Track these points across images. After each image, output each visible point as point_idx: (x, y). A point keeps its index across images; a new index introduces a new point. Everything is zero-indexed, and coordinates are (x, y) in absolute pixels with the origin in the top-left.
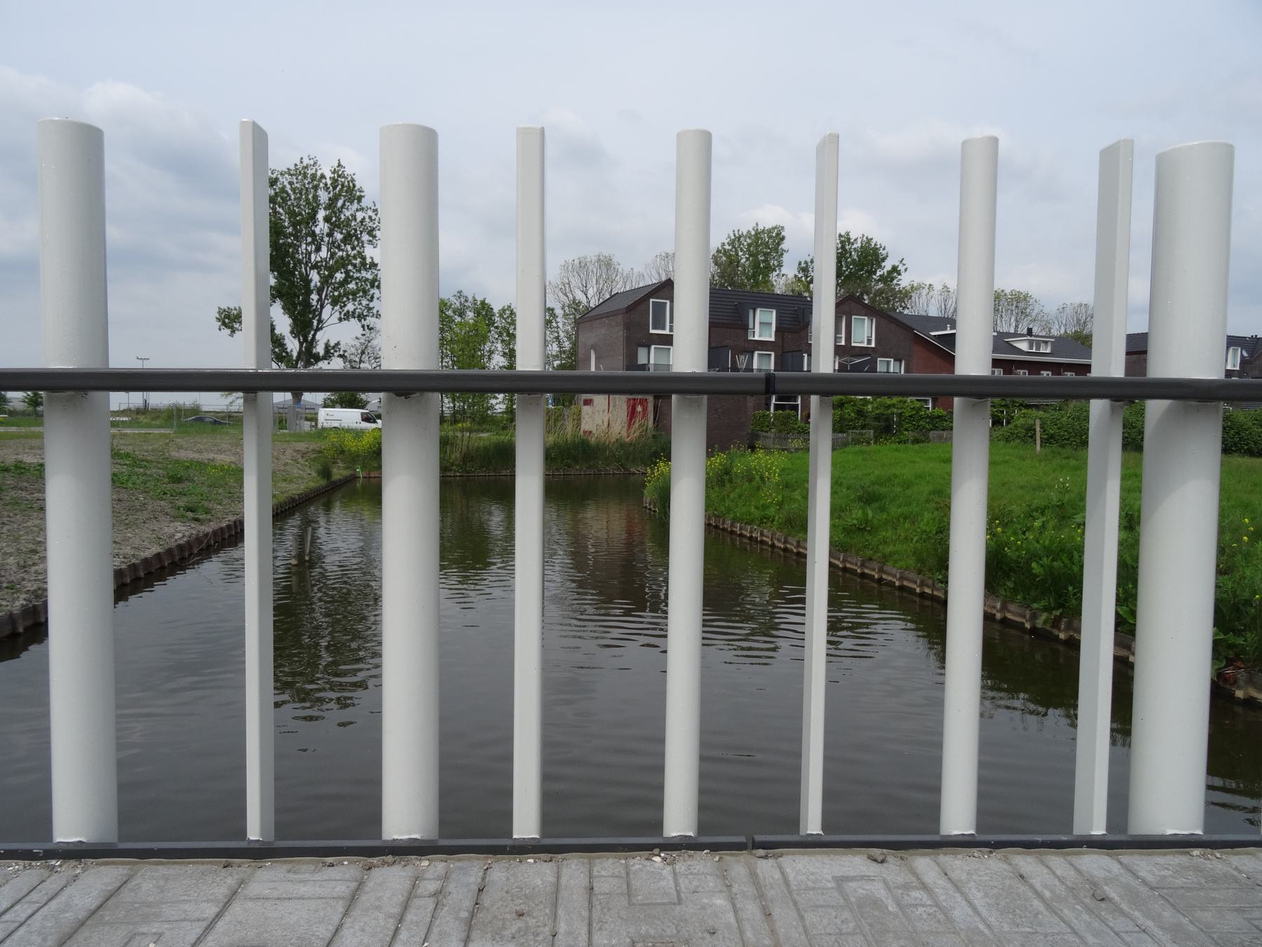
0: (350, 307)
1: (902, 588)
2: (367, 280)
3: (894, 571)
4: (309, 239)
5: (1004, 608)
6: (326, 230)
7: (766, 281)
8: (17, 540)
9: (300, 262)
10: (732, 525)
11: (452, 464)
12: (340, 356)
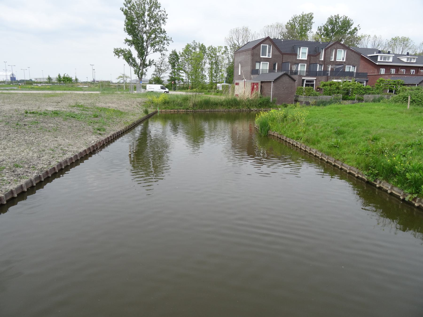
0: (157, 47)
1: (350, 173)
2: (162, 37)
3: (347, 166)
4: (143, 23)
5: (392, 188)
6: (148, 19)
7: (305, 35)
8: (39, 146)
9: (140, 31)
10: (286, 139)
11: (189, 107)
12: (154, 65)
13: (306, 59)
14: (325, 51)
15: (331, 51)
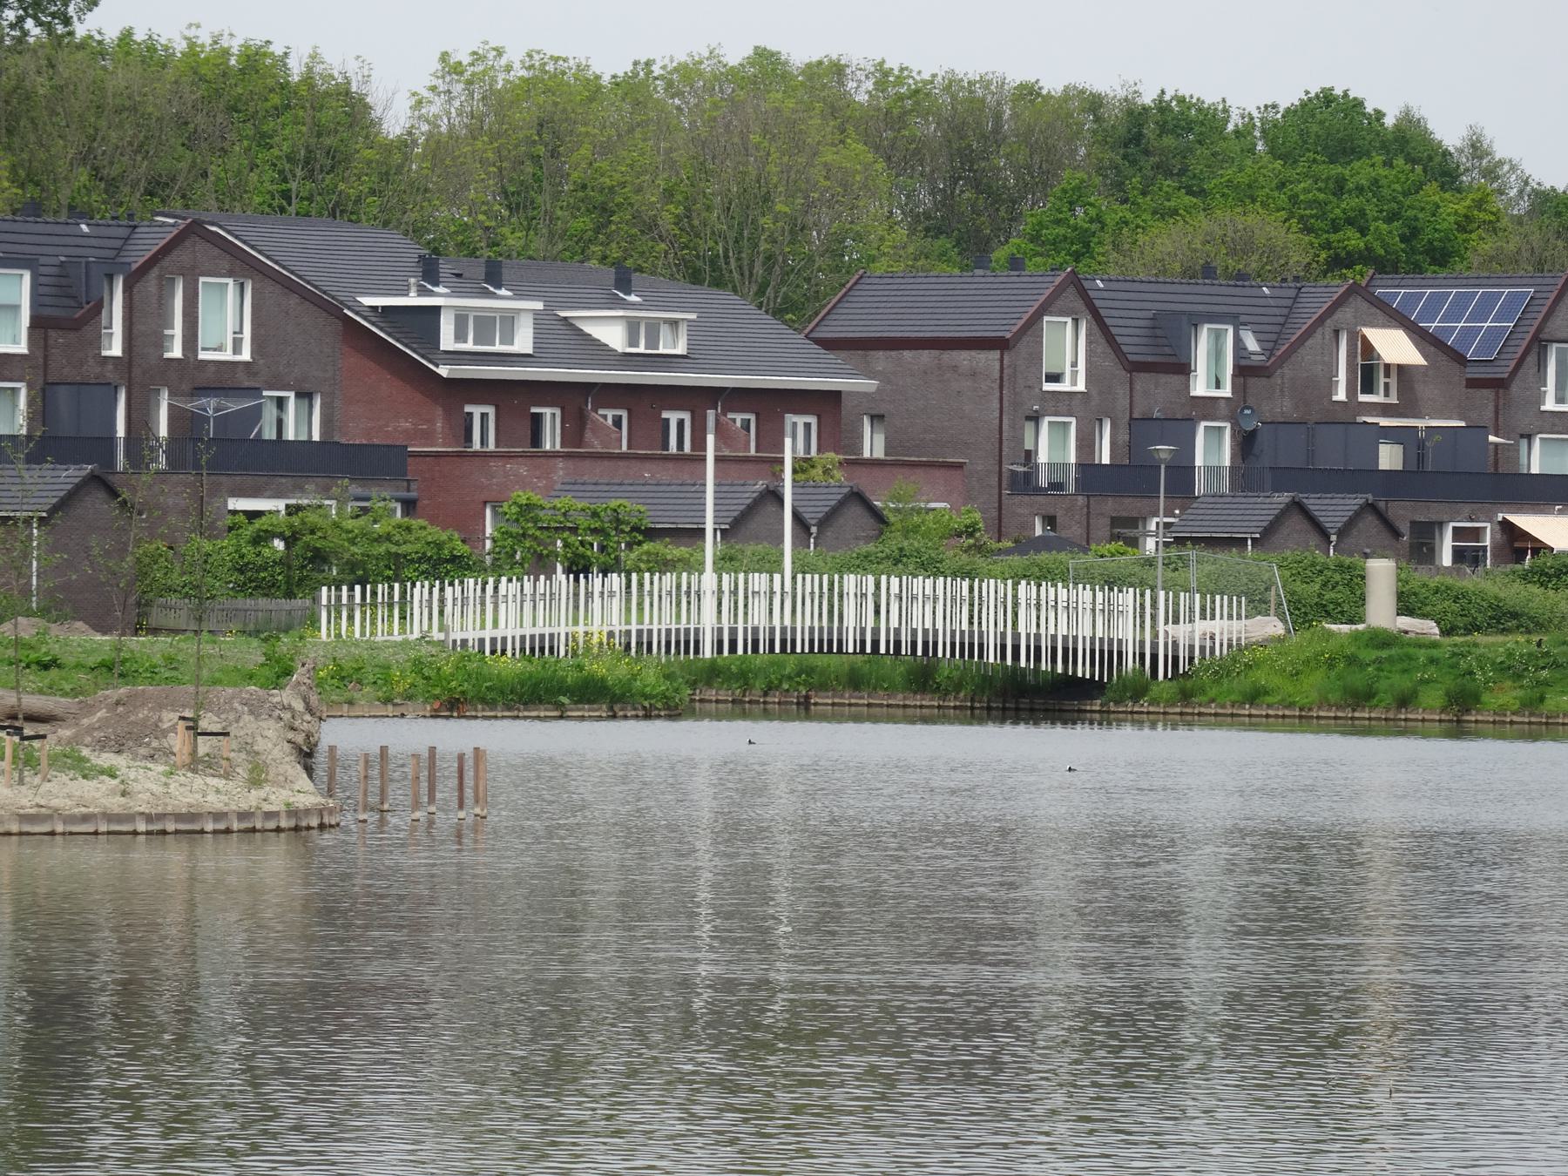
13: (22, 348)
14: (128, 290)
15: (161, 287)
